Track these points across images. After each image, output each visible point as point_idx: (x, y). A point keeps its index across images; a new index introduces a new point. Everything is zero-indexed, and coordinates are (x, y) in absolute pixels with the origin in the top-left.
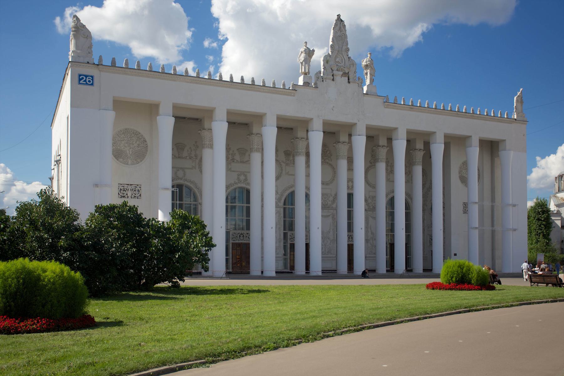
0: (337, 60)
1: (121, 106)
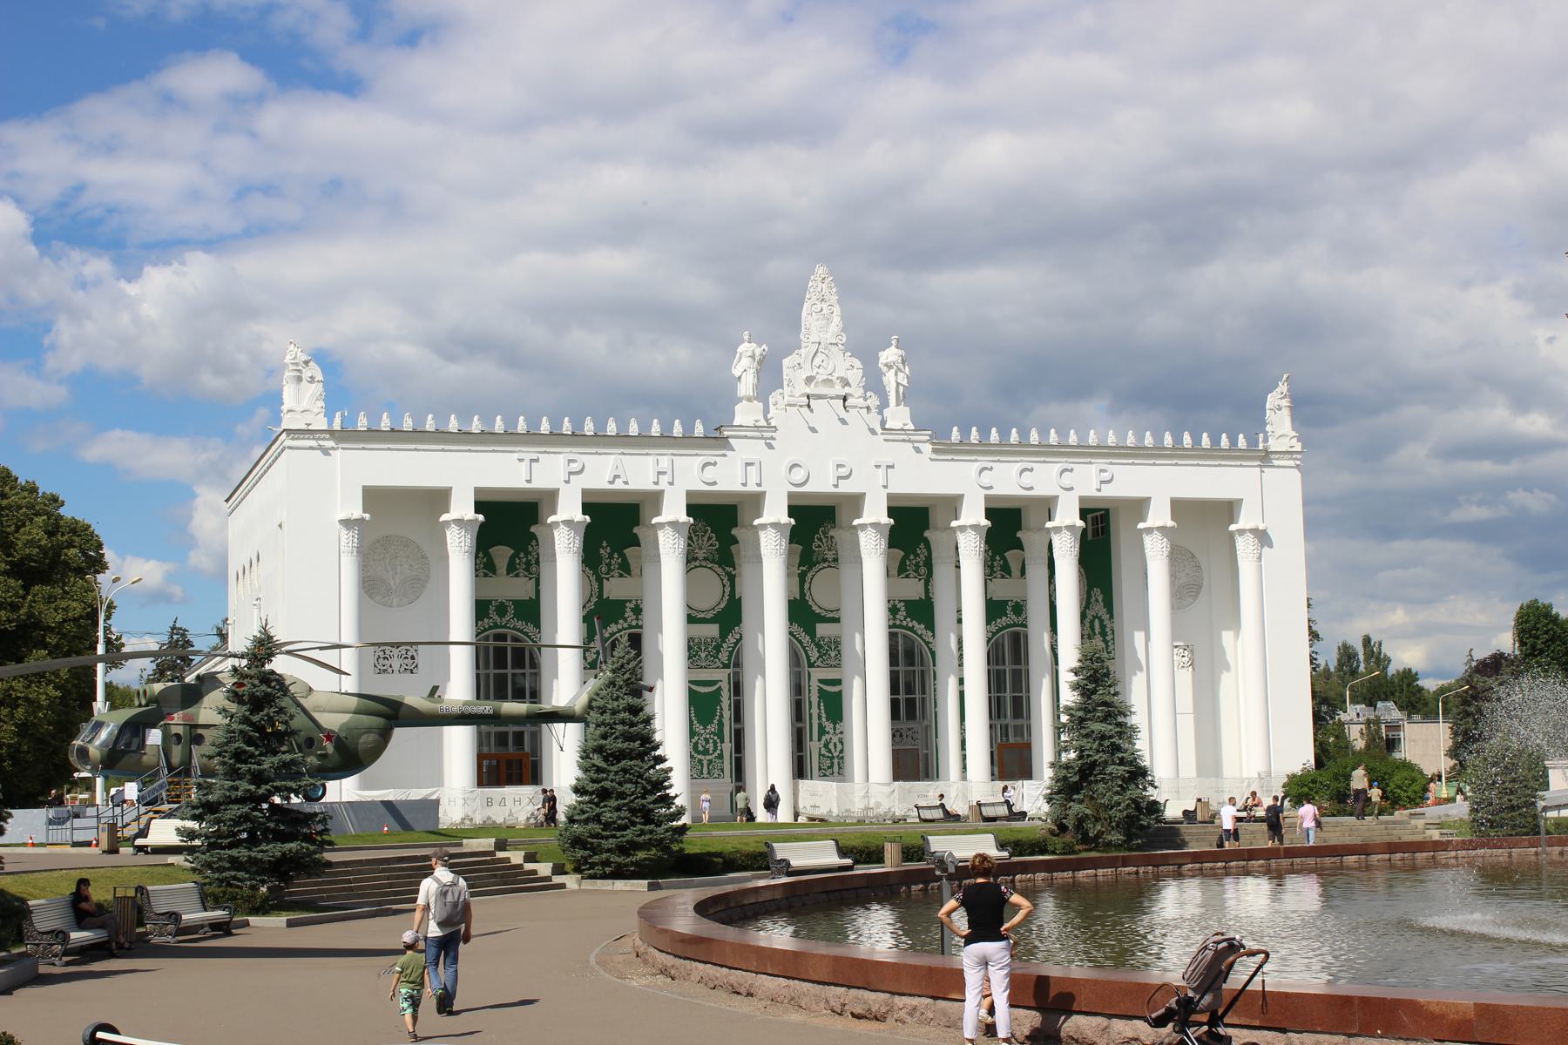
0: (817, 361)
1: (372, 496)
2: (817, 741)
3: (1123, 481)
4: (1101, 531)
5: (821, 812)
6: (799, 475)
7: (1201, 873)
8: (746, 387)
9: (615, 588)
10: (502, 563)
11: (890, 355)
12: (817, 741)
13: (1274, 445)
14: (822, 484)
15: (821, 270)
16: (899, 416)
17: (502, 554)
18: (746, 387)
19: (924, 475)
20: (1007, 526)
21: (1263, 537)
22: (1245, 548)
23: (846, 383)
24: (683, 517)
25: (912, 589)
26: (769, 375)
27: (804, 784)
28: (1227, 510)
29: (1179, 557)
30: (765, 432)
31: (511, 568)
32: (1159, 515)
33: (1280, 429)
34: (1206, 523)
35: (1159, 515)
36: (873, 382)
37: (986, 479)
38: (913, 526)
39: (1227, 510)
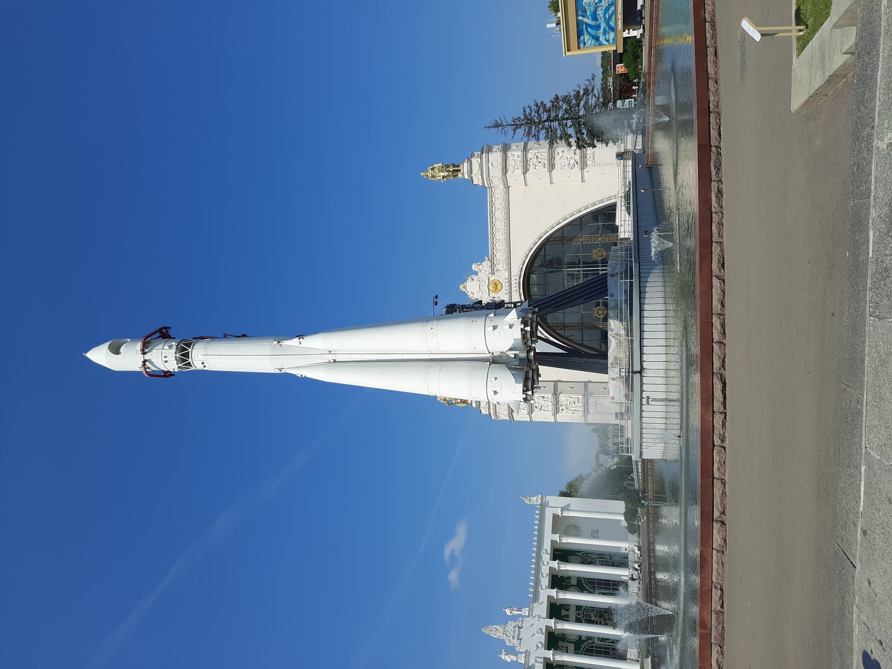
2: (610, 587)
3: (547, 546)
4: (561, 554)
5: (637, 654)
6: (540, 645)
7: (653, 544)
8: (514, 658)
9: (574, 582)
10: (567, 613)
11: (508, 612)
12: (610, 587)
13: (539, 503)
14: (542, 638)
15: (483, 630)
16: (525, 611)
17: (564, 613)
18: (514, 658)
19: (542, 608)
20: (559, 582)
21: (563, 509)
22: (566, 514)
23: (515, 627)
24: (551, 652)
25: (571, 647)
26: (511, 651)
27: (628, 656)
28: (555, 517)
29: (567, 534)
30: (527, 654)
31: (567, 610)
32: (556, 537)
33: (536, 500)
34: (561, 524)
35: (556, 537)
36: (514, 618)
37: (544, 588)
38: (556, 610)
39: (555, 517)
